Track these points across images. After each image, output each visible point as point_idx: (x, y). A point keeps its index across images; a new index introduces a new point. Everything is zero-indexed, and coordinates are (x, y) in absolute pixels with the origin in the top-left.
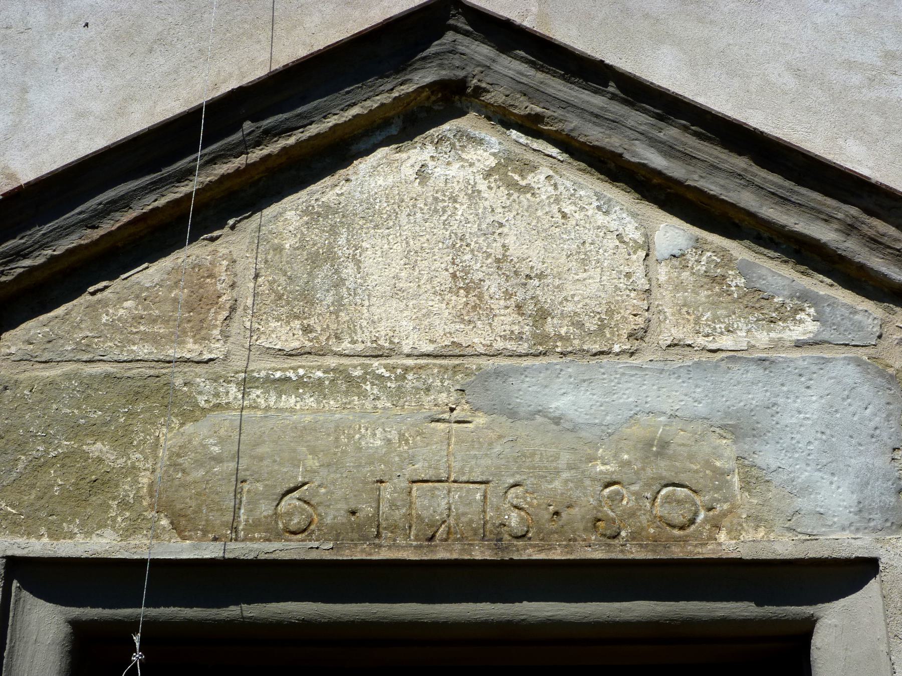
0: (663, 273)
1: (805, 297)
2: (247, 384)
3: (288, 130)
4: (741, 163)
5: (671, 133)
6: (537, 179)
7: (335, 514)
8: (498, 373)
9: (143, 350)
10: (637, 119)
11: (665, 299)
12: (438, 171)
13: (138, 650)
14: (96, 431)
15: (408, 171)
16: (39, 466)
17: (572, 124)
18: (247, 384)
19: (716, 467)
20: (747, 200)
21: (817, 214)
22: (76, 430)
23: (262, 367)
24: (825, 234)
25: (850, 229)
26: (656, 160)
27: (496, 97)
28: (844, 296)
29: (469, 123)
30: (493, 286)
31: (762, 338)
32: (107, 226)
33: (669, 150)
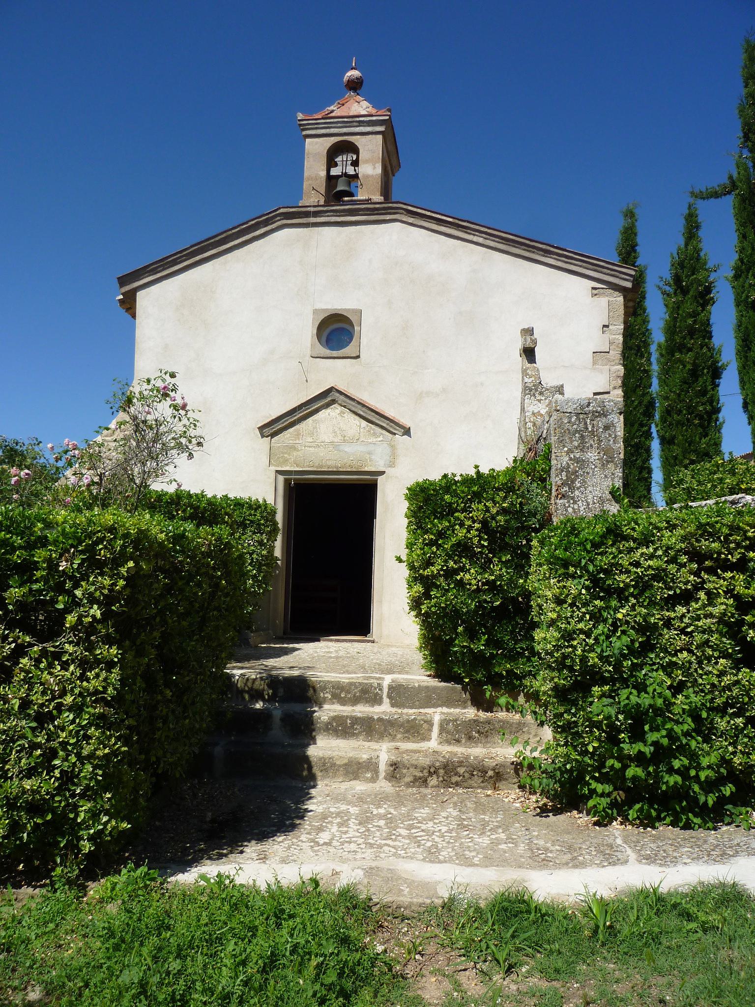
0: (362, 430)
1: (382, 434)
2: (305, 446)
3: (309, 408)
4: (373, 414)
5: (364, 409)
6: (345, 415)
7: (317, 464)
8: (339, 445)
9: (291, 442)
10: (359, 407)
11: (362, 434)
12: (331, 414)
13: (287, 706)
14: (286, 453)
15: (327, 414)
16: (278, 458)
17: (350, 407)
18: (305, 446)
19: (160, 496)
20: (374, 420)
21: (383, 422)
22: (283, 453)
23: (307, 444)
24: (384, 425)
25: (388, 424)
26: (362, 413)
27: (339, 402)
28: (387, 434)
29: (336, 405)
30: (338, 432)
31: (375, 440)
32: (285, 424)
33: (363, 412)
